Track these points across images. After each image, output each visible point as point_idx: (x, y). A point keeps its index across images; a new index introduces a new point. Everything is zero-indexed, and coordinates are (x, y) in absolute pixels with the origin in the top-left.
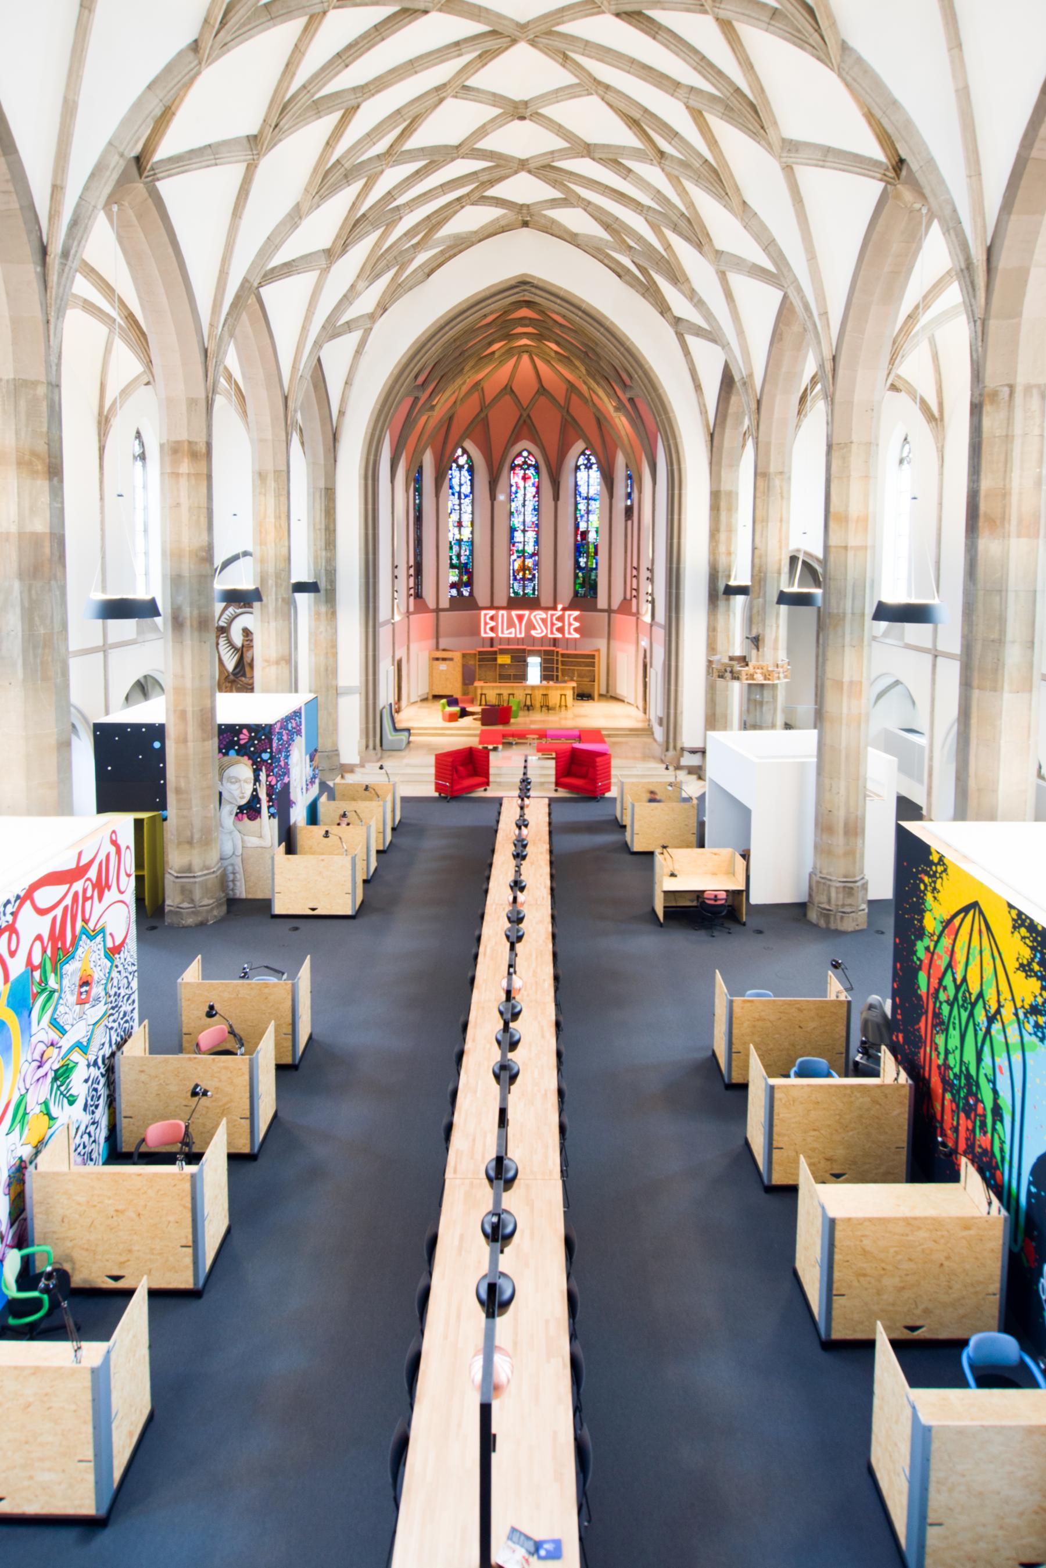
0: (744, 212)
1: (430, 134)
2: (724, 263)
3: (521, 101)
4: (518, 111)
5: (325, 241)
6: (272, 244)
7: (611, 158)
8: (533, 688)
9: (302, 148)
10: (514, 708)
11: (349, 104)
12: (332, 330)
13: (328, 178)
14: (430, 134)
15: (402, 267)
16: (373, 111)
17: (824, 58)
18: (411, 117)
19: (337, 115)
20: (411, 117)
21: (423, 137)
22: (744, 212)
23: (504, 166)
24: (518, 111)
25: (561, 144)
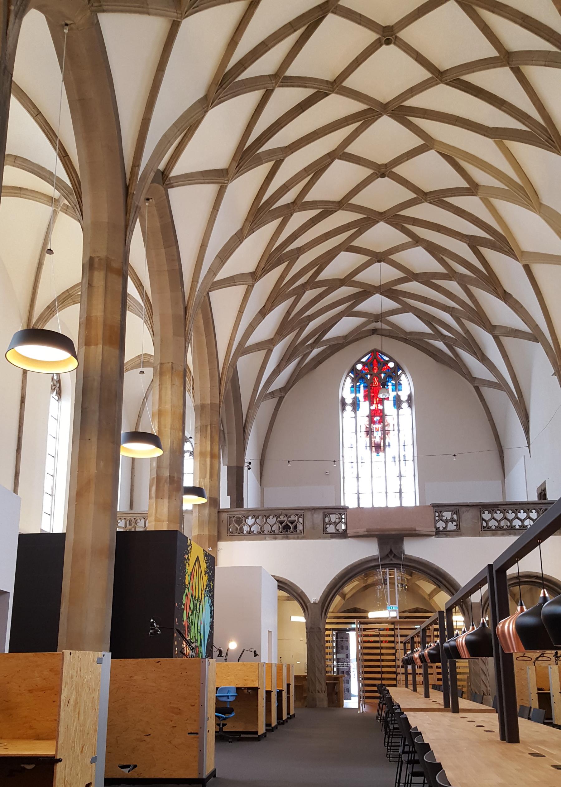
0: (506, 297)
1: (330, 272)
2: (498, 332)
3: (383, 164)
4: (383, 171)
5: (250, 267)
6: (213, 271)
7: (426, 278)
8: (467, 690)
9: (244, 189)
10: (191, 530)
11: (279, 156)
12: (242, 350)
13: (258, 214)
14: (330, 272)
15: (305, 356)
16: (293, 165)
17: (534, 210)
18: (317, 169)
19: (271, 164)
20: (317, 169)
21: (325, 275)
22: (506, 297)
23: (371, 218)
24: (383, 171)
25: (399, 274)
